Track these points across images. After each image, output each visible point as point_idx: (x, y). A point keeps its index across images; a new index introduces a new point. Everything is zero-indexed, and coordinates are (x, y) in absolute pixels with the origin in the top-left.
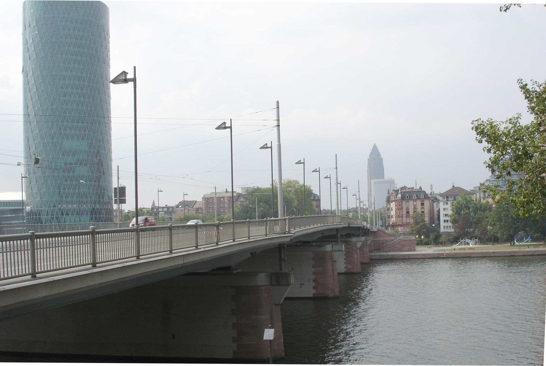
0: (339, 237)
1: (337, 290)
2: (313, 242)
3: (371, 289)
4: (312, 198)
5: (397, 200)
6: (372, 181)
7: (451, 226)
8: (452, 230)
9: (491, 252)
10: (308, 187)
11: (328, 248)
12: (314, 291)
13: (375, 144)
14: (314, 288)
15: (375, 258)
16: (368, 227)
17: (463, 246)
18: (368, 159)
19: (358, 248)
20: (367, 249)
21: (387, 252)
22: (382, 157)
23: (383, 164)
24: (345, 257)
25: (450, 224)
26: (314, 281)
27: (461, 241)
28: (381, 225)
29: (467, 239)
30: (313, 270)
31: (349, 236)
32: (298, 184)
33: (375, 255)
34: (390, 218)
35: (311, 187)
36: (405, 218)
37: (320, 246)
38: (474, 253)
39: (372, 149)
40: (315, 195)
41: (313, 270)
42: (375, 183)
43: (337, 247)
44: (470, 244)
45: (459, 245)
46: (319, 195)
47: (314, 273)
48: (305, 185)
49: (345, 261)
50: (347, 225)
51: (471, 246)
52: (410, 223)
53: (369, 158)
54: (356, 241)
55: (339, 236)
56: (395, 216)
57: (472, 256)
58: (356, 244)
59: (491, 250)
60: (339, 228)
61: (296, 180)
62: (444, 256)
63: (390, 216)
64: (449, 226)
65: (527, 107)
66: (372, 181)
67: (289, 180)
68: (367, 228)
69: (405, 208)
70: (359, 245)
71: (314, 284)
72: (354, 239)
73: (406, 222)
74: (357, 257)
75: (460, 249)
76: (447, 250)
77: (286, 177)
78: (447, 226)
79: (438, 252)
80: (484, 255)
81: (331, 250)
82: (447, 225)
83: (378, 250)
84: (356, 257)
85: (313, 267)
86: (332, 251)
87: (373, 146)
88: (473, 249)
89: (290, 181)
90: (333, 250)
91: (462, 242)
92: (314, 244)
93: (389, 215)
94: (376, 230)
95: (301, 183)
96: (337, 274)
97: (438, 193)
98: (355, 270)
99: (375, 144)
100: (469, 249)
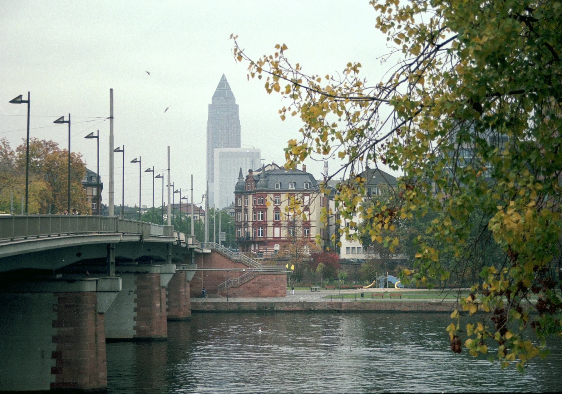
0: (112, 263)
1: (103, 375)
2: (58, 271)
3: (43, 357)
4: (85, 180)
5: (258, 191)
6: (217, 151)
7: (349, 248)
8: (362, 256)
9: (432, 302)
10: (77, 156)
11: (89, 286)
12: (53, 378)
13: (224, 79)
14: (54, 371)
15: (205, 308)
16: (189, 244)
17: (382, 290)
18: (209, 105)
19: (163, 287)
20: (185, 291)
21: (228, 296)
22: (237, 103)
23: (238, 117)
24: (135, 305)
25: (357, 244)
26: (55, 355)
27: (377, 278)
28: (223, 243)
29: (389, 274)
30: (54, 331)
31: (146, 260)
32: (53, 149)
33: (205, 304)
34: (241, 228)
35: (81, 158)
36: (272, 228)
37: (72, 281)
38: (400, 304)
39: (218, 86)
40: (89, 172)
41: (54, 331)
42: (222, 155)
43: (105, 284)
44: (394, 285)
45: (374, 287)
46: (96, 172)
47: (55, 339)
48: (71, 152)
49: (135, 314)
50: (137, 239)
51: (396, 289)
52: (282, 239)
53: (211, 103)
54: (159, 272)
55: (112, 260)
56: (272, 223)
57: (397, 309)
58: (159, 279)
59: (435, 300)
60: (113, 244)
61: (51, 142)
62: (341, 307)
63: (243, 224)
64: (358, 247)
65: (284, 45)
66: (217, 151)
67: (36, 140)
68: (187, 245)
69: (271, 208)
70: (166, 280)
71: (53, 363)
72: (156, 269)
73: (274, 237)
74: (161, 306)
75: (373, 295)
76: (347, 296)
77: (38, 135)
78: (353, 248)
79: (329, 300)
80: (420, 309)
81: (95, 290)
82: (353, 246)
83: (213, 293)
84: (158, 305)
85: (55, 324)
86: (96, 292)
87: (220, 78)
88: (400, 295)
89: (39, 142)
90: (99, 289)
91: (379, 281)
92: (59, 276)
93: (241, 222)
94: (209, 251)
95: (63, 146)
96: (104, 341)
97: (339, 180)
98: (155, 334)
99: (224, 79)
100: (392, 295)
